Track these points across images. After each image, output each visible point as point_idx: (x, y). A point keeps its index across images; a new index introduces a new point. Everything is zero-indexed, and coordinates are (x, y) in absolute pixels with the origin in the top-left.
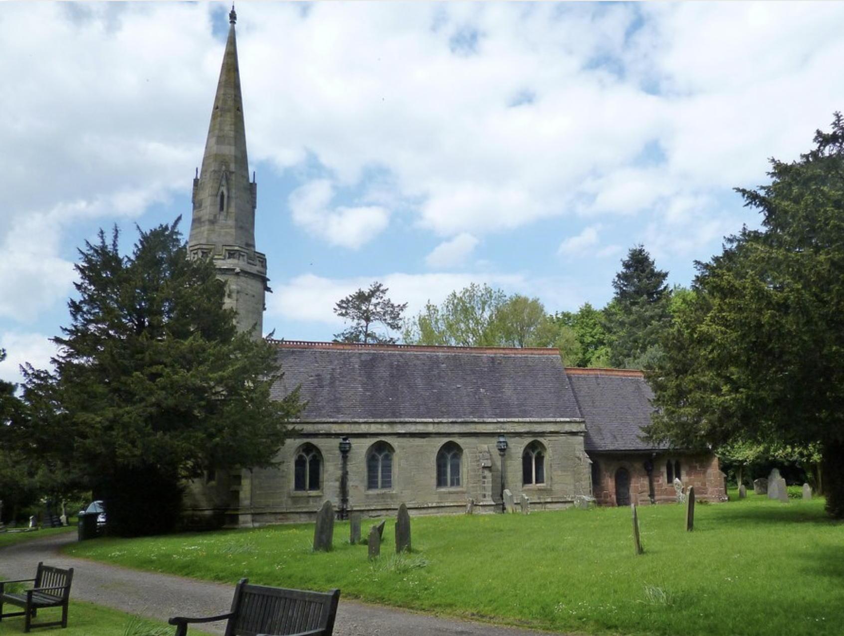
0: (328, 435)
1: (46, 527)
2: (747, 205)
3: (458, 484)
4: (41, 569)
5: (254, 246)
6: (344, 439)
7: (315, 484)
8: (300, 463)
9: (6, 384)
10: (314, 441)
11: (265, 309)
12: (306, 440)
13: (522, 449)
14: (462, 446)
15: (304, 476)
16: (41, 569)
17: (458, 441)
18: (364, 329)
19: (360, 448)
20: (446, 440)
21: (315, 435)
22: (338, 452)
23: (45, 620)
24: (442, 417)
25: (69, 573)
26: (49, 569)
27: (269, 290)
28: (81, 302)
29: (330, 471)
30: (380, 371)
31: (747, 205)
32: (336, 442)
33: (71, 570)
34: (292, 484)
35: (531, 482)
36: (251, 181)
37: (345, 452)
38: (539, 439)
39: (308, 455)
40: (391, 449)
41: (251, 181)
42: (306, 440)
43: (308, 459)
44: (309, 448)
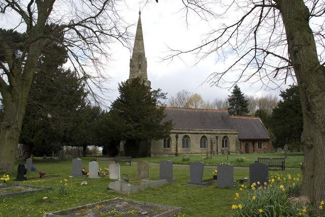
7: (169, 146)
19: (181, 137)
20: (203, 135)
29: (173, 142)
37: (177, 137)
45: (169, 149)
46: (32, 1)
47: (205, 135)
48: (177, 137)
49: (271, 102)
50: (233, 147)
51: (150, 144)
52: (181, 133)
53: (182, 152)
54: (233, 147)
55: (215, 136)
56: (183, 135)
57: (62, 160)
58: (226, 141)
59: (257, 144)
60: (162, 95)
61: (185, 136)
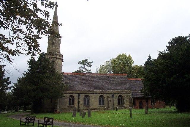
0: (76, 93)
1: (160, 107)
2: (28, 62)
3: (104, 104)
4: (45, 118)
7: (73, 104)
12: (71, 95)
13: (98, 98)
15: (70, 101)
16: (45, 118)
19: (82, 96)
20: (101, 95)
21: (73, 93)
22: (78, 97)
23: (30, 125)
24: (100, 90)
25: (53, 119)
26: (46, 118)
28: (46, 32)
29: (76, 101)
30: (79, 77)
31: (28, 62)
33: (53, 118)
34: (68, 104)
35: (120, 104)
37: (79, 97)
45: (73, 106)
46: (4, 49)
47: (88, 95)
48: (79, 97)
49: (107, 67)
50: (127, 104)
51: (57, 102)
52: (83, 94)
53: (83, 108)
54: (127, 104)
55: (111, 95)
56: (84, 95)
57: (57, 113)
58: (122, 99)
59: (150, 101)
60: (89, 63)
61: (87, 96)
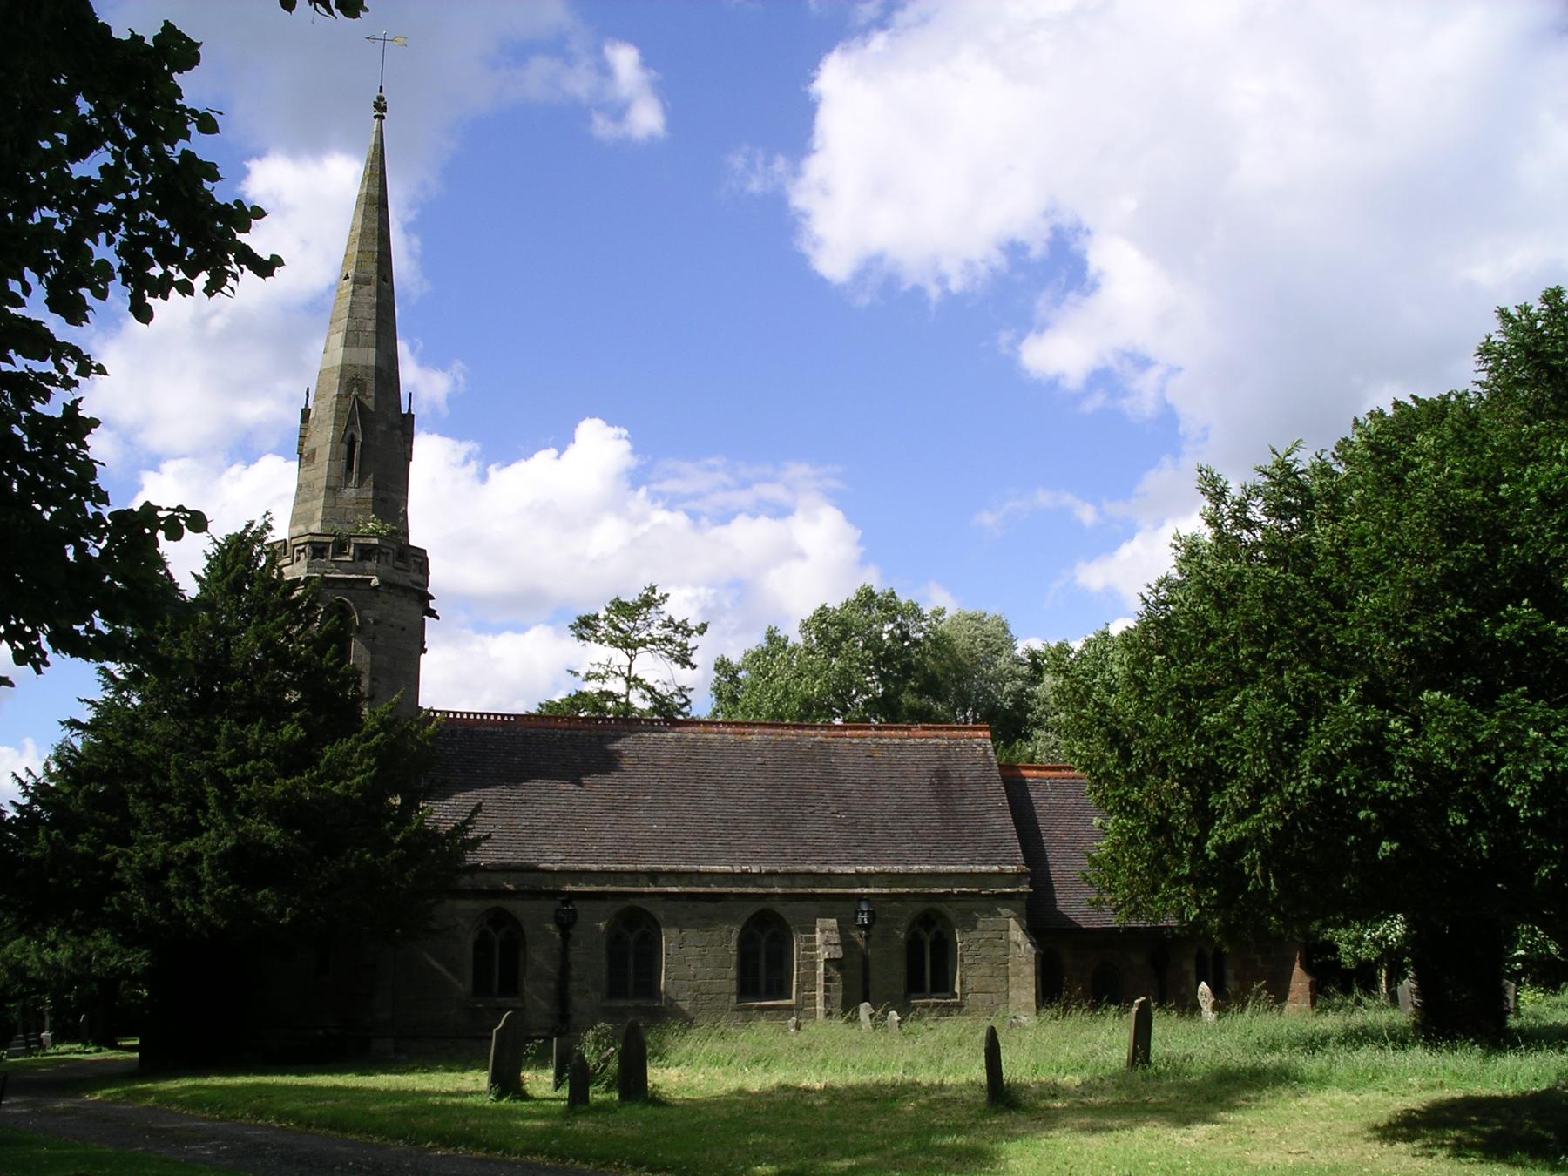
5: (406, 534)
6: (565, 903)
7: (511, 985)
8: (482, 945)
9: (538, 717)
10: (509, 905)
11: (425, 651)
12: (494, 903)
14: (789, 919)
17: (780, 908)
18: (625, 670)
27: (432, 614)
32: (549, 907)
36: (404, 411)
38: (937, 905)
39: (927, 930)
40: (941, 915)
41: (404, 411)
42: (494, 903)
43: (928, 939)
44: (499, 918)
